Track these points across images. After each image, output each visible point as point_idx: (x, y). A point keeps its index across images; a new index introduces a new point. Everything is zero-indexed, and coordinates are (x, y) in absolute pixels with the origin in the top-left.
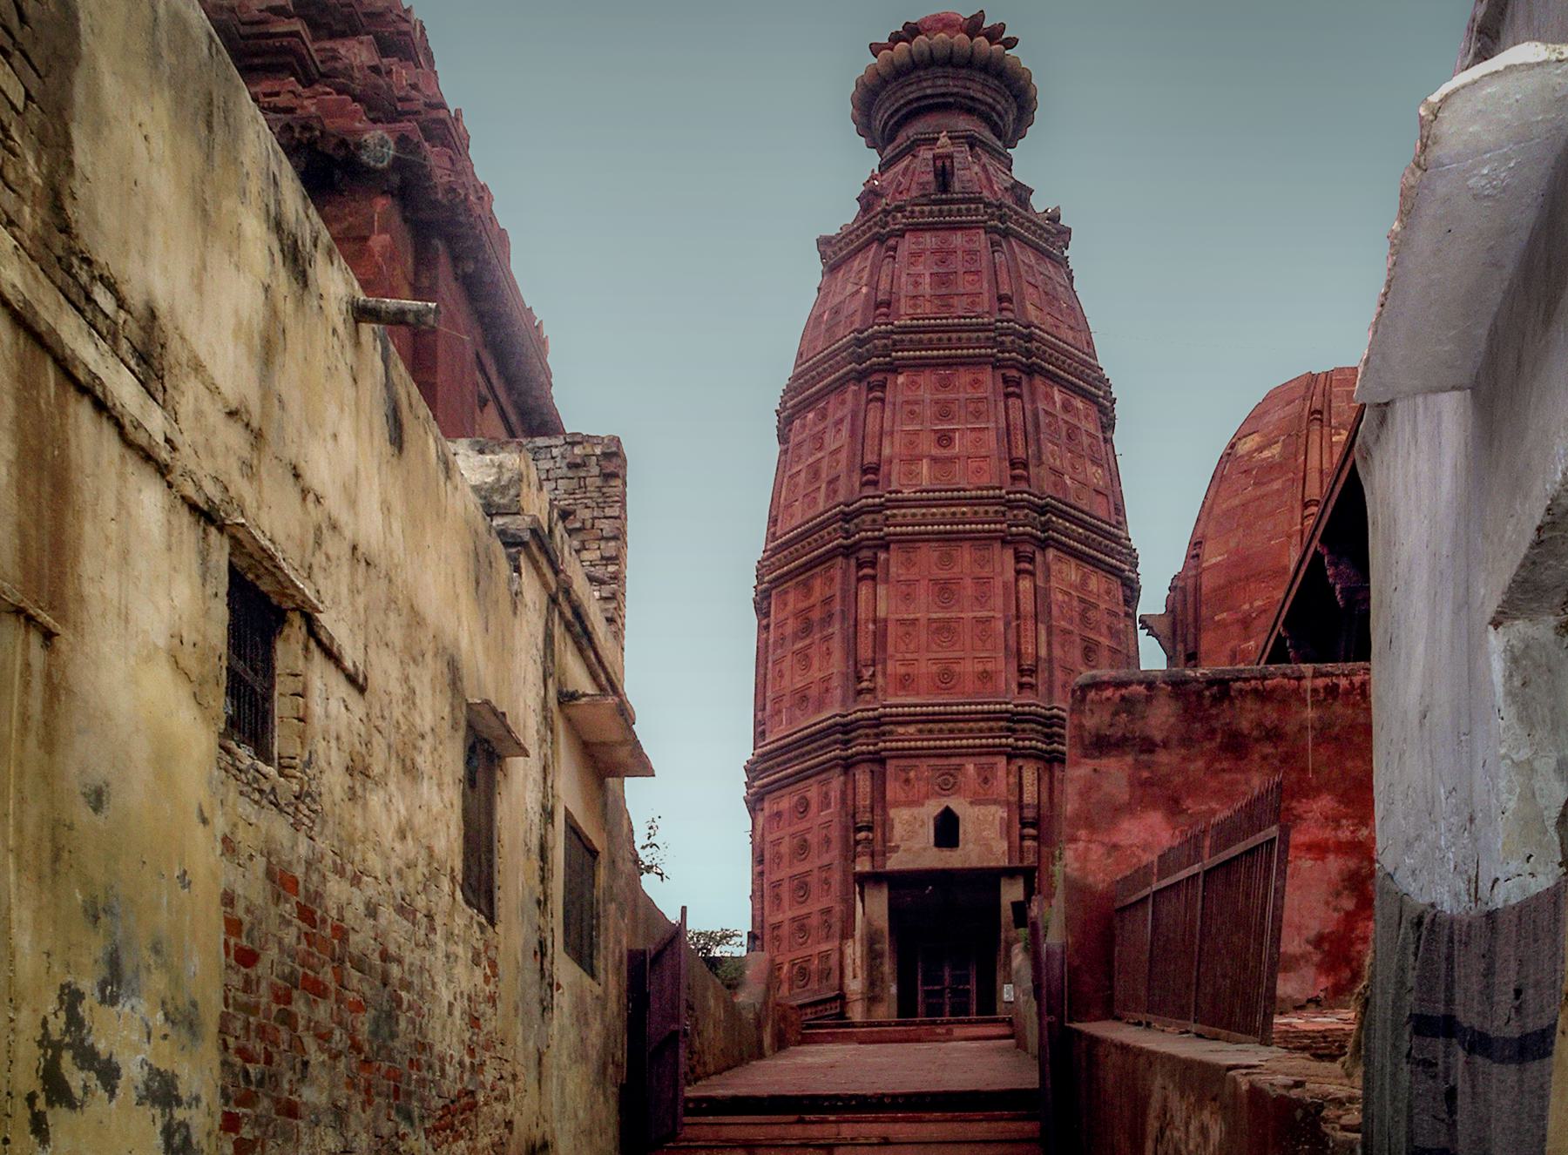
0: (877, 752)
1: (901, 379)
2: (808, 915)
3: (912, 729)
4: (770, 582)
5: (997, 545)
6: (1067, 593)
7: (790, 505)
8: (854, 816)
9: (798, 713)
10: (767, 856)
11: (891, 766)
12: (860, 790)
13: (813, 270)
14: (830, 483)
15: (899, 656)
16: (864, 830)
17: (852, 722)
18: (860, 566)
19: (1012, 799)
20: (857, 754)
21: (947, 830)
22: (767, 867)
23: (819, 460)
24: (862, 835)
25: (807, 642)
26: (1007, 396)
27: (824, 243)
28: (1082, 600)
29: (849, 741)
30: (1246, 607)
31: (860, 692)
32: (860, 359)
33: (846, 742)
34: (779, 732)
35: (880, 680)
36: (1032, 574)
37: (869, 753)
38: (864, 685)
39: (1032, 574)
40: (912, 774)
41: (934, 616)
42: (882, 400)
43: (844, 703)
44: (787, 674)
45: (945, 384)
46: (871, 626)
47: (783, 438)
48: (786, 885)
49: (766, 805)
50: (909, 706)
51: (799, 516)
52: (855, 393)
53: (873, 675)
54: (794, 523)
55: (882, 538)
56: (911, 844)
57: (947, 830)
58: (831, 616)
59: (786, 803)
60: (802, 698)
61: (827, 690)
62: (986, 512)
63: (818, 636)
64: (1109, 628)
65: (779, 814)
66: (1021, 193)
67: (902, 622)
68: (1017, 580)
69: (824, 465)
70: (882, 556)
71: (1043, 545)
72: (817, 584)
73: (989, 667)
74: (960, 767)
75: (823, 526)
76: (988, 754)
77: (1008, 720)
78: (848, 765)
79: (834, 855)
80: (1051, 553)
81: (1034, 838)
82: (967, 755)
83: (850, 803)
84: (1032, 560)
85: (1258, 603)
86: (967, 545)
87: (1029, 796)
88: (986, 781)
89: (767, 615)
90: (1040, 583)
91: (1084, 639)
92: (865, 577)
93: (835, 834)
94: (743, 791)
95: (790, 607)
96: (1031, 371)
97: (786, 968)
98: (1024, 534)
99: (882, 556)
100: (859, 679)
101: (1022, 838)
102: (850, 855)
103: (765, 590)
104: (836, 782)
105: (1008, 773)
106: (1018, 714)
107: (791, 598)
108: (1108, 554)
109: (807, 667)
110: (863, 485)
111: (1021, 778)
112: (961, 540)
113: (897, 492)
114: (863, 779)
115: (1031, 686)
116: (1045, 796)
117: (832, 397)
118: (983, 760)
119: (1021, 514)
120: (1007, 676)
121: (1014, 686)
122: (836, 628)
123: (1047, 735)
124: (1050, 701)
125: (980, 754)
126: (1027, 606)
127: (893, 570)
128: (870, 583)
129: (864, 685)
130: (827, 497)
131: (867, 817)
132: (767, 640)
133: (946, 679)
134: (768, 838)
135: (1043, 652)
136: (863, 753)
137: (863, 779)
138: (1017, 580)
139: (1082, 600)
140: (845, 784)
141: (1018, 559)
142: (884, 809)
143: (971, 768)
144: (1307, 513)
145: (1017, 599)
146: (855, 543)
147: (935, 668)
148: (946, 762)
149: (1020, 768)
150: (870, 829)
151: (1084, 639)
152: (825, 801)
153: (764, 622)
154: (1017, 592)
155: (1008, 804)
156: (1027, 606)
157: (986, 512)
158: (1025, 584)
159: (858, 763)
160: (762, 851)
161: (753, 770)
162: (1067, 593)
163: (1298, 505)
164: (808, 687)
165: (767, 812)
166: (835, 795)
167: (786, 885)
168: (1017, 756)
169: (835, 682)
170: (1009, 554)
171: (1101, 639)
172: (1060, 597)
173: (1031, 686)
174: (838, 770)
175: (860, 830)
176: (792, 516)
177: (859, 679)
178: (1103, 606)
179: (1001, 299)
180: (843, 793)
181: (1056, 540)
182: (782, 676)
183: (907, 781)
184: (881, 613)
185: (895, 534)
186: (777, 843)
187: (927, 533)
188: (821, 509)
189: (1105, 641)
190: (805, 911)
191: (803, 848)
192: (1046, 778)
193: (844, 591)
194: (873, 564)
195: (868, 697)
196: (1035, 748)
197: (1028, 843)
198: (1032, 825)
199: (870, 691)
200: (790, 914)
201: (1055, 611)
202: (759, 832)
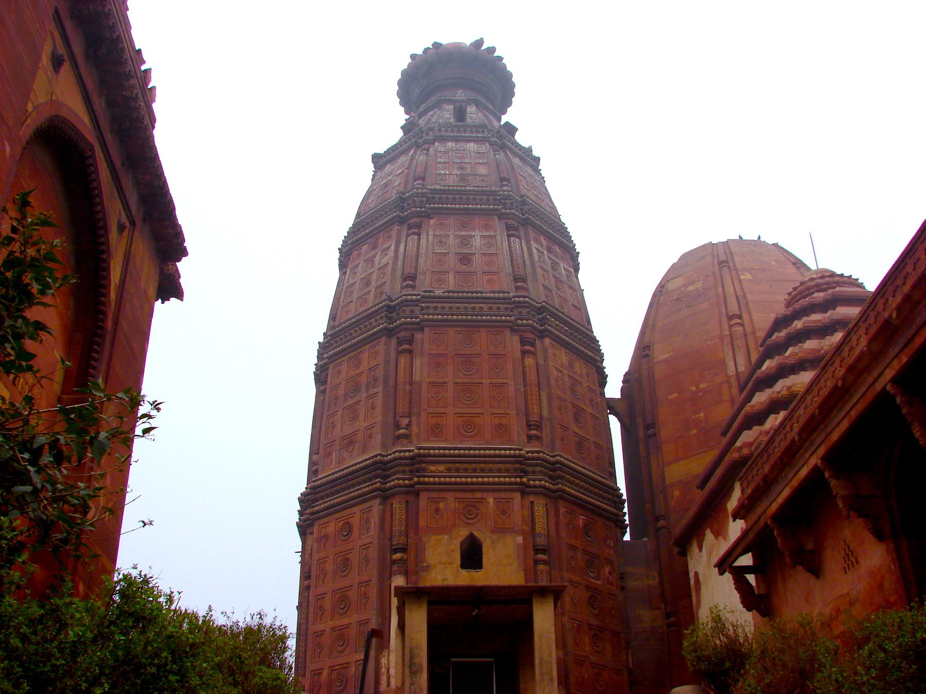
0: (412, 486)
1: (432, 222)
2: (347, 626)
3: (441, 468)
4: (329, 358)
5: (508, 332)
6: (560, 371)
7: (347, 305)
8: (391, 539)
9: (345, 454)
10: (314, 573)
11: (424, 496)
12: (397, 517)
13: (369, 168)
14: (377, 288)
15: (431, 410)
16: (401, 551)
17: (391, 461)
18: (400, 343)
19: (526, 528)
20: (395, 487)
21: (472, 556)
22: (313, 581)
23: (371, 274)
24: (398, 556)
25: (356, 399)
26: (509, 236)
27: (376, 158)
28: (570, 377)
29: (389, 476)
30: (694, 388)
31: (399, 437)
32: (403, 209)
33: (385, 477)
34: (328, 472)
35: (415, 428)
36: (534, 354)
37: (406, 486)
38: (402, 431)
39: (534, 354)
40: (441, 505)
41: (459, 381)
42: (410, 352)
43: (384, 445)
44: (339, 425)
45: (464, 226)
46: (408, 387)
47: (343, 265)
48: (329, 596)
49: (315, 529)
50: (439, 449)
51: (354, 310)
52: (399, 232)
53: (409, 424)
54: (349, 316)
55: (418, 324)
56: (444, 569)
57: (472, 556)
58: (376, 380)
59: (332, 527)
60: (349, 441)
61: (370, 436)
62: (499, 308)
63: (364, 395)
64: (591, 401)
65: (326, 537)
66: (511, 129)
67: (432, 384)
68: (523, 358)
69: (375, 276)
70: (418, 336)
71: (542, 334)
72: (365, 356)
73: (504, 421)
74: (481, 501)
75: (369, 317)
76: (505, 490)
77: (520, 463)
78: (386, 496)
79: (372, 572)
80: (547, 341)
81: (545, 562)
82: (488, 491)
83: (387, 527)
84: (533, 344)
85: (702, 386)
86: (483, 330)
87: (540, 526)
88: (504, 512)
89: (325, 382)
90: (541, 362)
91: (574, 405)
92: (404, 351)
93: (373, 553)
94: (296, 518)
95: (343, 374)
96: (526, 223)
97: (325, 672)
98: (528, 325)
99: (418, 336)
100: (398, 427)
101: (536, 562)
102: (385, 575)
103: (325, 364)
104: (376, 506)
105: (523, 507)
106: (528, 459)
107: (344, 368)
108: (589, 353)
109: (355, 418)
110: (403, 288)
111: (532, 510)
112: (479, 327)
113: (430, 292)
114: (398, 505)
115: (538, 438)
116: (552, 528)
117: (382, 234)
118: (502, 495)
119: (525, 311)
120: (518, 429)
121: (524, 438)
122: (379, 389)
123: (551, 477)
124: (553, 451)
125: (499, 490)
126: (532, 377)
127: (426, 346)
128: (416, 237)
129: (402, 431)
130: (375, 297)
131: (403, 540)
132: (323, 401)
133: (469, 426)
134: (316, 556)
135: (545, 413)
136: (400, 486)
137: (398, 505)
138: (523, 358)
139: (570, 377)
140: (384, 511)
141: (523, 342)
142: (417, 533)
143: (491, 500)
144: (732, 322)
145: (524, 373)
146: (397, 327)
147: (460, 420)
148: (469, 495)
149: (532, 502)
150: (404, 550)
151: (574, 405)
152: (368, 523)
153: (322, 388)
154: (524, 367)
155: (524, 533)
156: (532, 377)
157: (499, 308)
158: (529, 361)
159: (393, 495)
160: (310, 571)
161: (306, 501)
162: (560, 371)
163: (724, 319)
164: (354, 434)
165: (315, 535)
166: (375, 520)
167: (329, 596)
168: (529, 493)
169: (378, 429)
170: (516, 339)
171: (585, 408)
172: (555, 373)
173: (538, 438)
174: (377, 501)
175: (395, 551)
176: (347, 312)
177: (398, 427)
178: (585, 385)
179: (502, 180)
180: (382, 519)
181: (551, 332)
182: (334, 427)
183: (437, 510)
184: (417, 377)
185: (429, 320)
186: (323, 561)
187: (453, 321)
188: (371, 305)
189: (589, 410)
190: (345, 621)
191: (345, 563)
192: (552, 513)
193: (387, 361)
194: (410, 341)
195: (405, 441)
196: (544, 487)
197: (541, 567)
198: (544, 551)
199: (407, 436)
200: (331, 624)
201: (553, 382)
202: (308, 552)
